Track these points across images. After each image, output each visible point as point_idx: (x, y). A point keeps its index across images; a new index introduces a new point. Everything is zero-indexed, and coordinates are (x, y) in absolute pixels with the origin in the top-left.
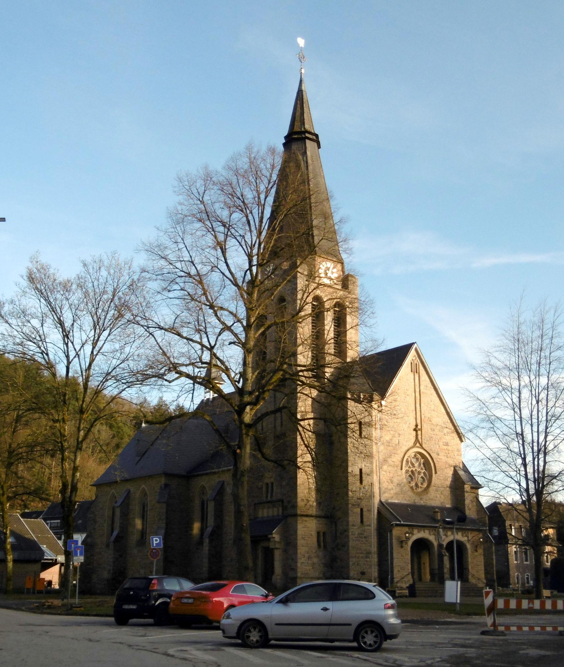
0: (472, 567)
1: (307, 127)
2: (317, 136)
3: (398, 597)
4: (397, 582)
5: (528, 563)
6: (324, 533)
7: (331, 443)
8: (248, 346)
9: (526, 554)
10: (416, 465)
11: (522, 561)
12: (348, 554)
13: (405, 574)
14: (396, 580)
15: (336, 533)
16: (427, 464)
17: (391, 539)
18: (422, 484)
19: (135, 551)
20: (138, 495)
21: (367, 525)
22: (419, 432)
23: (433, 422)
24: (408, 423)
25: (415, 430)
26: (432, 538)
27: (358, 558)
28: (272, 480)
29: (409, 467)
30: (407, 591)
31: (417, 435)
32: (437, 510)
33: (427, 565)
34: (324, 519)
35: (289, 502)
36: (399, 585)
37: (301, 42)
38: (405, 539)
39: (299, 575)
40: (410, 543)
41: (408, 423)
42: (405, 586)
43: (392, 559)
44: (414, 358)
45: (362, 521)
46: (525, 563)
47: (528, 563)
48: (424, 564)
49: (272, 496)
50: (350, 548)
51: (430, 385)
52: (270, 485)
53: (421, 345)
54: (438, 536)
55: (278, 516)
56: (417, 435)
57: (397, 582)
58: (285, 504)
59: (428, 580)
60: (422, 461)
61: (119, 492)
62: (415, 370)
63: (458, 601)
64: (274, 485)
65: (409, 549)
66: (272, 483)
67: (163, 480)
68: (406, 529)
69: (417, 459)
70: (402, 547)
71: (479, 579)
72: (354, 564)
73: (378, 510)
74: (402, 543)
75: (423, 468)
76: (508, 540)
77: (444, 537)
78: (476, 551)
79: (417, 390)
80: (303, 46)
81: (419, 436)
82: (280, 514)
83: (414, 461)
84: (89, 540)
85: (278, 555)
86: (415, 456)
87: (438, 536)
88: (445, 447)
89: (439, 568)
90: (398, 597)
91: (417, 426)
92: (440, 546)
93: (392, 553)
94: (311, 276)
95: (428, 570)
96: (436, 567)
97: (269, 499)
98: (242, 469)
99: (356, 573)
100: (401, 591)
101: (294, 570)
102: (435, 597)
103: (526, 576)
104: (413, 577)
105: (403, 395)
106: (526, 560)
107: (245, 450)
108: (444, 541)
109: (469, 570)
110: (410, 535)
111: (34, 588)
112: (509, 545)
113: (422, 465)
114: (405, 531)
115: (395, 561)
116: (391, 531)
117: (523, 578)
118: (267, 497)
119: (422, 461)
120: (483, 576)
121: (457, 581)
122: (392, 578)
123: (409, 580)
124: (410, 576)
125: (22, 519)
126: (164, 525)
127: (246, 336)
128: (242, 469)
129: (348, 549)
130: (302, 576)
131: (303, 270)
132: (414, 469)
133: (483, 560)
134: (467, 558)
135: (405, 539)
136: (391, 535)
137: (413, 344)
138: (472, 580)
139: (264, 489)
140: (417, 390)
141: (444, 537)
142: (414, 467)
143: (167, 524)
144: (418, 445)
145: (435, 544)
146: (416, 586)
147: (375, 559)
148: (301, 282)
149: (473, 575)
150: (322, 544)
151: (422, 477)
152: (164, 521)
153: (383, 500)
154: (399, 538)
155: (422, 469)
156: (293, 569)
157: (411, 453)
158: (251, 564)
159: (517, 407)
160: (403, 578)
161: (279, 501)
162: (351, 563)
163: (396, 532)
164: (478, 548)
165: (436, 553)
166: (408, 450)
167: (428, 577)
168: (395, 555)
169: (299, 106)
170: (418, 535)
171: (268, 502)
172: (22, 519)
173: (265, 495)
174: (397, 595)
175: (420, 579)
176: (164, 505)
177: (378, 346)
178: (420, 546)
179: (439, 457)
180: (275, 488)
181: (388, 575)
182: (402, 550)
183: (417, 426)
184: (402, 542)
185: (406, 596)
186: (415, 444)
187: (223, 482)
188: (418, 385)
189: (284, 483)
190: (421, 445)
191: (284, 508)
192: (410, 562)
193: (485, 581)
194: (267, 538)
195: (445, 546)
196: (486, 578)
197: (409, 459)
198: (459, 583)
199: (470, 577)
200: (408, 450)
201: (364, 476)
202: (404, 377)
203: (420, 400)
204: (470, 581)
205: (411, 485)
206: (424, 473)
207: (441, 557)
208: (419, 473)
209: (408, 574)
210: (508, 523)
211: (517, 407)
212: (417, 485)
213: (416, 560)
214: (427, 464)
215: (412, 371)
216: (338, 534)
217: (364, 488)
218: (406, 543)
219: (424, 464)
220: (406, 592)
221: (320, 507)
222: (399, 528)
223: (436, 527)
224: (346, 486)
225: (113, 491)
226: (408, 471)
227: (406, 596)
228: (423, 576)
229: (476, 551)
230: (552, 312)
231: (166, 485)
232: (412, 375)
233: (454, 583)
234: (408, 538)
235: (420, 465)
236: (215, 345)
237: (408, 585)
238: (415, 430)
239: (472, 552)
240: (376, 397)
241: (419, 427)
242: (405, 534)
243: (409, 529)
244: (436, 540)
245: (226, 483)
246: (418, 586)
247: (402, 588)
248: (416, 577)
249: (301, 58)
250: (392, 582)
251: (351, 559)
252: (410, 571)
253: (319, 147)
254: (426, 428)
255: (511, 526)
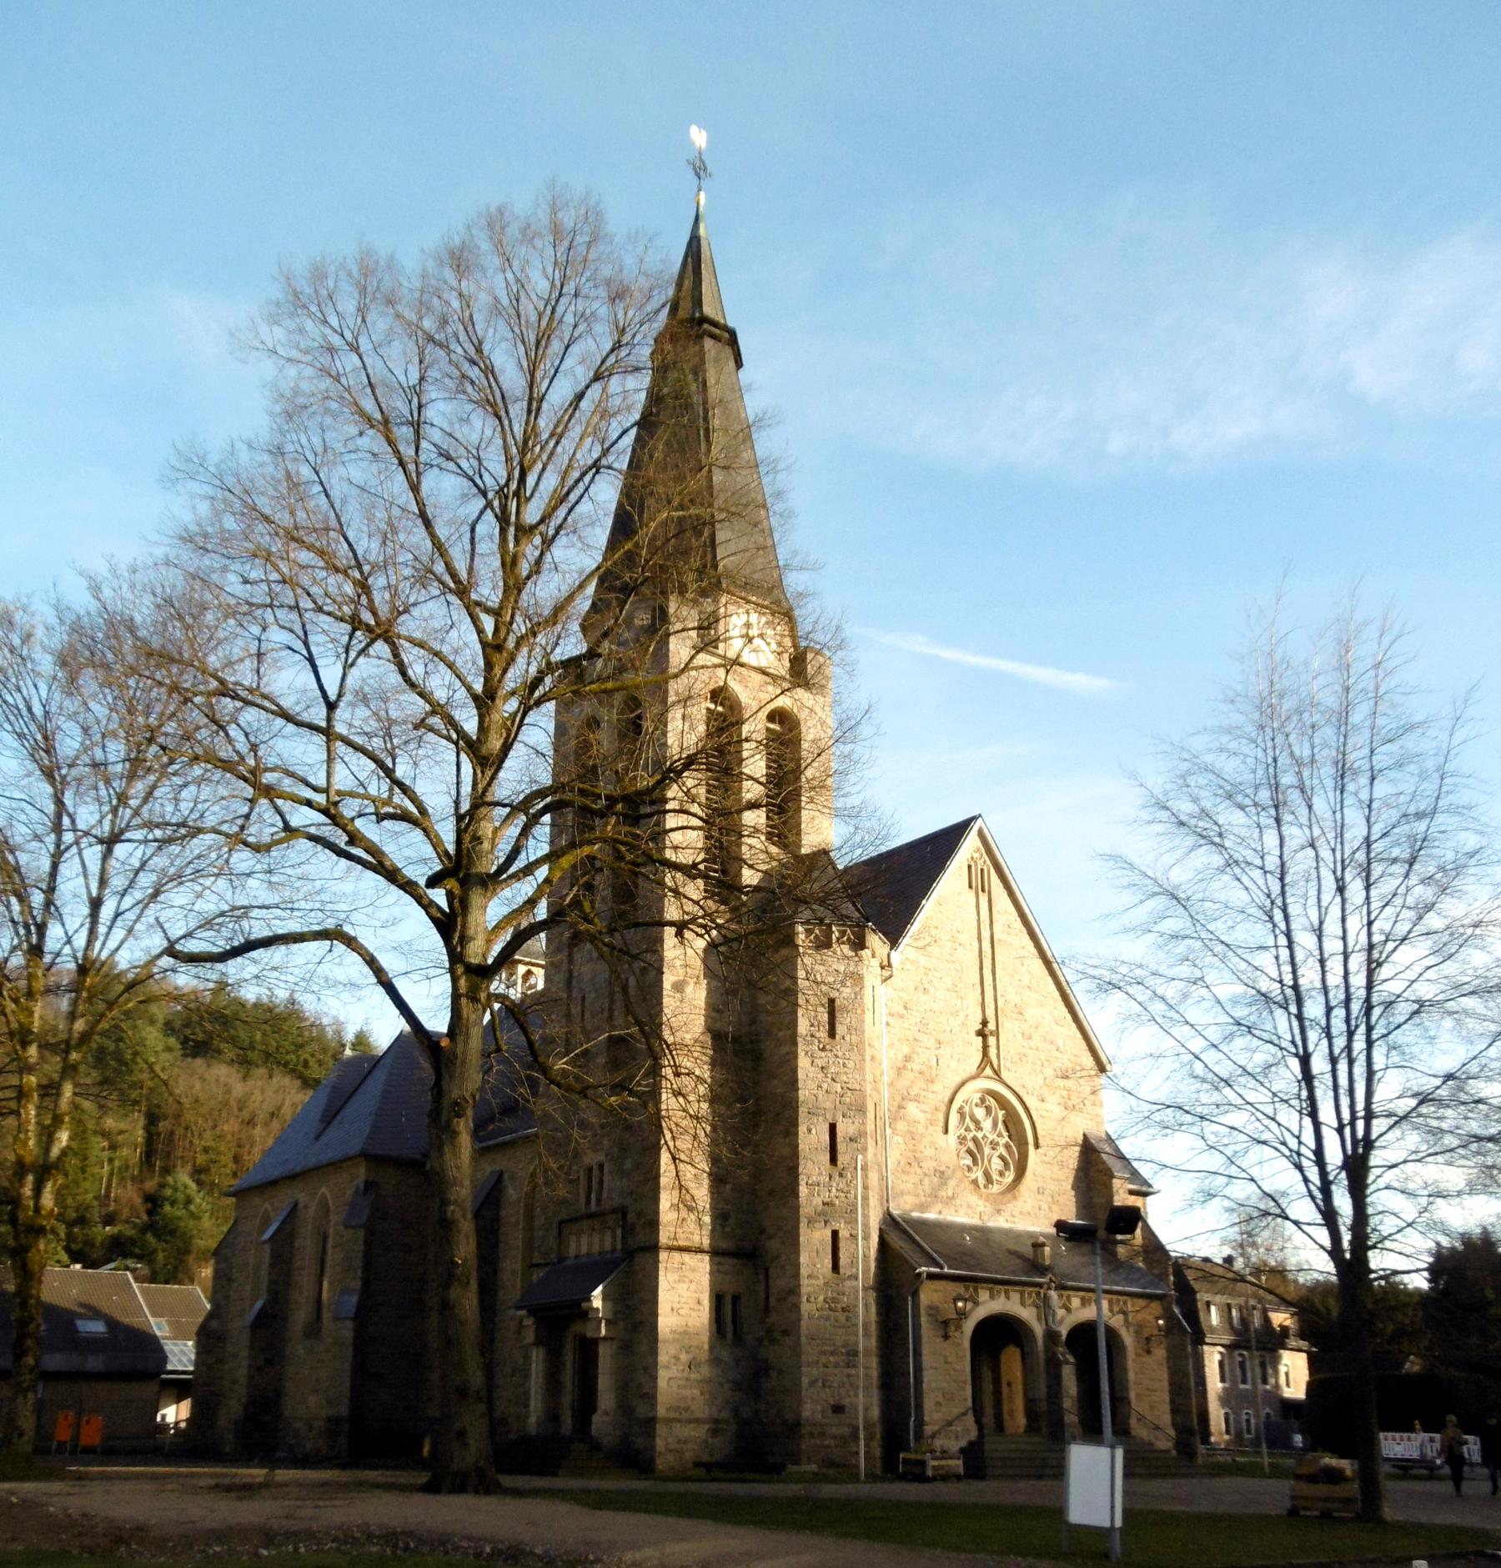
0: (1138, 1395)
1: (708, 310)
2: (732, 334)
3: (934, 1479)
4: (933, 1436)
5: (1248, 1387)
6: (736, 1299)
7: (757, 1057)
8: (484, 751)
9: (1242, 1365)
10: (987, 1124)
11: (1234, 1383)
12: (799, 1355)
13: (956, 1411)
14: (928, 1430)
15: (767, 1298)
16: (1012, 1124)
17: (917, 1315)
18: (1001, 1174)
19: (301, 1351)
20: (311, 1212)
21: (850, 1277)
22: (992, 1040)
23: (1027, 1015)
24: (962, 1015)
25: (981, 1033)
26: (1027, 1314)
27: (825, 1366)
28: (600, 1157)
29: (967, 1129)
30: (960, 1462)
31: (985, 1047)
32: (1042, 1239)
33: (1018, 1388)
34: (735, 1261)
35: (639, 1215)
36: (938, 1443)
37: (699, 137)
38: (954, 1316)
39: (661, 1411)
40: (969, 1326)
41: (962, 1015)
42: (954, 1446)
43: (918, 1369)
44: (976, 855)
45: (836, 1267)
46: (1242, 1386)
47: (1248, 1387)
48: (1009, 1384)
49: (599, 1201)
50: (803, 1339)
51: (1018, 924)
52: (595, 1172)
53: (994, 824)
54: (1044, 1307)
55: (614, 1250)
56: (985, 1047)
57: (933, 1436)
58: (631, 1217)
59: (1021, 1430)
60: (1001, 1113)
61: (274, 1208)
62: (977, 884)
63: (1118, 1523)
64: (606, 1171)
65: (967, 1344)
66: (601, 1166)
67: (362, 1172)
68: (959, 1288)
69: (988, 1110)
70: (946, 1337)
71: (1157, 1428)
72: (812, 1383)
73: (881, 1238)
74: (946, 1327)
75: (1005, 1134)
76: (1204, 1335)
77: (1061, 1313)
78: (1149, 1352)
79: (986, 935)
80: (704, 146)
81: (992, 1052)
82: (619, 1246)
83: (980, 1113)
84: (214, 1324)
85: (605, 1353)
86: (983, 1100)
87: (1044, 1307)
88: (1061, 1083)
89: (1049, 1395)
90: (934, 1479)
91: (985, 1023)
92: (1051, 1336)
93: (918, 1354)
94: (708, 635)
95: (1019, 1403)
96: (1042, 1392)
97: (593, 1207)
98: (455, 1094)
99: (819, 1408)
100: (943, 1462)
101: (650, 1397)
102: (1040, 1477)
103: (1245, 1417)
104: (978, 1422)
105: (949, 944)
106: (1244, 1382)
107: (466, 1043)
108: (1061, 1321)
109: (1129, 1403)
110: (969, 1305)
111: (76, 1438)
112: (1206, 1348)
113: (1001, 1126)
114: (954, 1294)
115: (927, 1376)
116: (915, 1294)
117: (1238, 1422)
118: (588, 1202)
119: (1001, 1113)
120: (1166, 1419)
121: (1113, 1447)
122: (920, 1423)
123: (967, 1431)
124: (970, 1419)
125: (135, 1285)
126: (357, 1284)
127: (481, 722)
128: (455, 1094)
129: (798, 1343)
130: (673, 1415)
131: (683, 614)
132: (980, 1135)
133: (1166, 1376)
134: (1125, 1370)
135: (954, 1316)
136: (916, 1305)
137: (974, 819)
138: (1139, 1431)
139: (583, 1181)
140: (986, 935)
141: (1061, 1313)
142: (981, 1129)
143: (366, 1283)
144: (988, 1071)
145: (1039, 1330)
146: (987, 1447)
147: (869, 1368)
148: (679, 649)
149: (1141, 1418)
150: (729, 1328)
151: (1001, 1157)
152: (359, 1273)
153: (895, 1212)
154: (934, 1311)
155: (1000, 1135)
156: (646, 1394)
157: (972, 1092)
158: (477, 1379)
159: (1276, 910)
160: (950, 1424)
161: (614, 1211)
162: (805, 1381)
163: (929, 1295)
164: (1153, 1343)
165: (1042, 1356)
166: (963, 1084)
167: (1021, 1420)
168: (926, 1359)
169: (690, 267)
170: (989, 1305)
171: (590, 1216)
172: (135, 1285)
173: (583, 1200)
174: (930, 1473)
175: (1000, 1427)
176: (361, 1233)
177: (886, 838)
178: (997, 1335)
179: (1044, 1105)
180: (606, 1178)
181: (909, 1416)
182: (945, 1344)
183: (985, 1023)
184: (946, 1323)
185: (958, 1478)
186: (981, 1068)
187: (501, 1173)
188: (989, 951)
189: (628, 1164)
190: (997, 1073)
191: (629, 1230)
192: (969, 1378)
193: (1172, 1433)
194: (580, 1311)
195: (1064, 1338)
196: (1174, 1425)
197: (967, 1109)
198: (1119, 1453)
199: (1133, 1421)
200: (963, 1084)
201: (841, 1147)
202: (949, 898)
203: (1009, 1087)
204: (1133, 1433)
205: (973, 1176)
206: (1007, 1146)
207: (1053, 1366)
208: (994, 1145)
209: (964, 1414)
210: (1202, 1297)
211: (1276, 910)
212: (987, 1175)
213: (987, 1374)
214: (1012, 1124)
215: (970, 887)
216: (772, 1301)
217: (841, 1175)
218: (959, 1327)
219: (1004, 1122)
220: (957, 1465)
221: (723, 1226)
222: (937, 1284)
223: (1040, 1285)
224: (793, 1171)
225: (267, 1205)
226: (965, 1138)
227: (958, 1478)
228: (1006, 1416)
229: (1149, 1352)
230: (1372, 632)
231: (369, 1185)
232: (971, 895)
233: (1102, 1453)
234: (962, 1315)
235: (995, 1125)
236: (340, 696)
237: (963, 1443)
238: (981, 1033)
239: (1137, 1355)
240: (875, 941)
241: (991, 1026)
242: (955, 1300)
243: (967, 1288)
244: (1039, 1319)
245: (506, 1176)
246: (995, 1447)
247: (945, 1454)
248: (989, 1419)
249: (700, 169)
250: (919, 1435)
251: (804, 1370)
252: (969, 1403)
253: (739, 364)
254: (1008, 1028)
255: (1208, 1304)
